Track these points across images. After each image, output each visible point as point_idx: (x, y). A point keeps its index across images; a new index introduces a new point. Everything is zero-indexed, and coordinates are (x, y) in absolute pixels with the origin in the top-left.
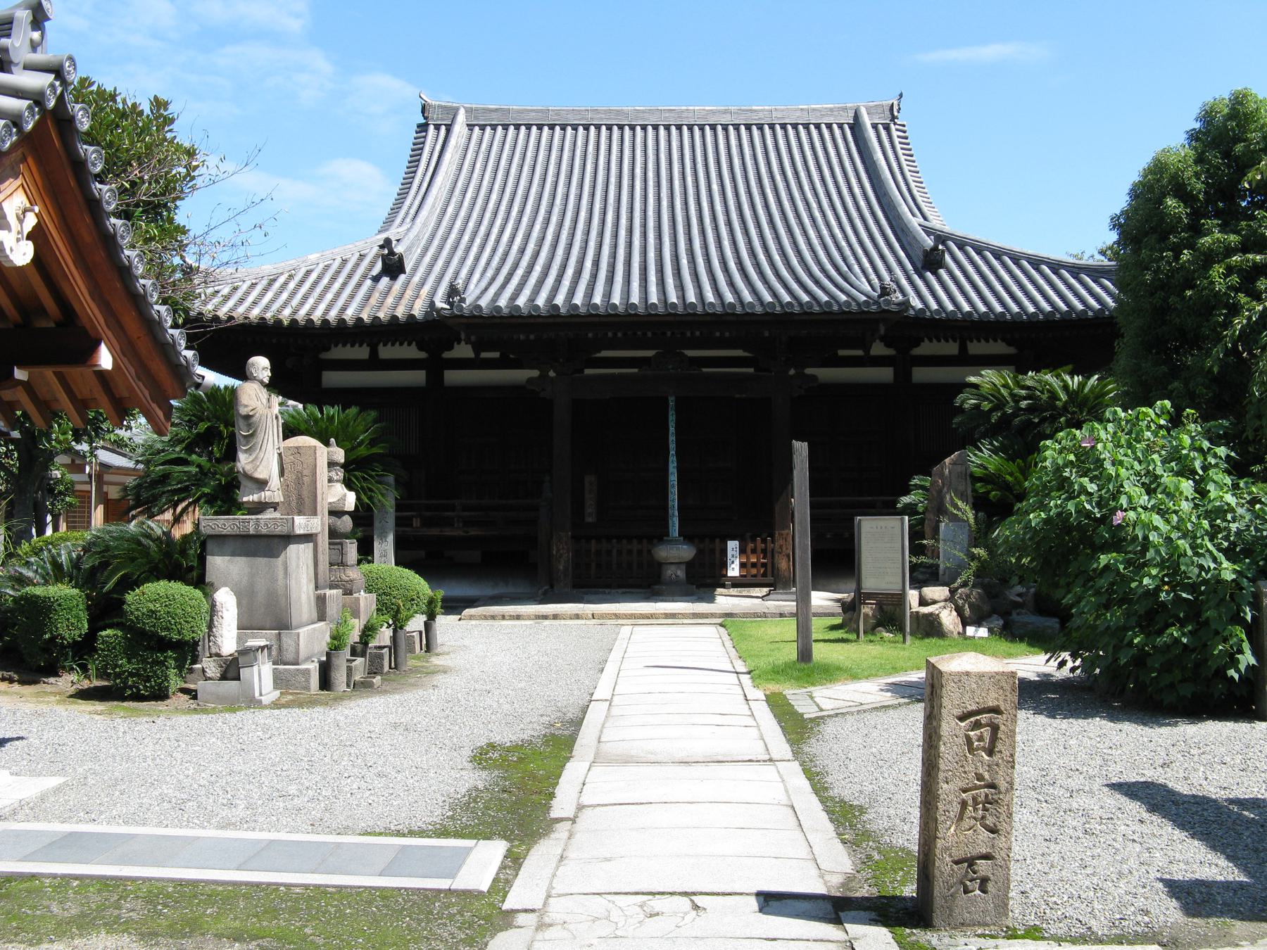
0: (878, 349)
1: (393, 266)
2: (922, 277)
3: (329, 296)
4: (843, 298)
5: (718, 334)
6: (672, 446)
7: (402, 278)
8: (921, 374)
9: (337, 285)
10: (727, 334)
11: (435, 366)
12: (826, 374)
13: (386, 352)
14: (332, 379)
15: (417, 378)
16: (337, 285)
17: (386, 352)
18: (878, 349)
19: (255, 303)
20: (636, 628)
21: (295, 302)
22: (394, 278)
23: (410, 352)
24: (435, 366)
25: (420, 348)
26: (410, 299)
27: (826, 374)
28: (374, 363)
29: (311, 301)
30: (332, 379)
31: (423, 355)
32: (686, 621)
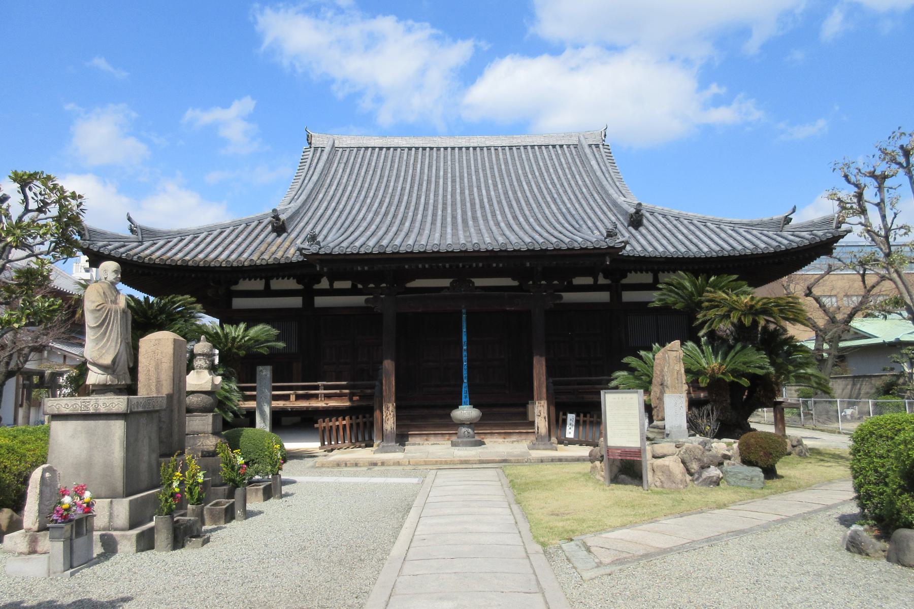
0: (602, 280)
1: (636, 220)
2: (765, 243)
3: (233, 246)
4: (554, 240)
5: (494, 265)
6: (465, 374)
7: (285, 235)
8: (628, 296)
9: (239, 240)
10: (501, 265)
11: (308, 294)
12: (569, 297)
13: (276, 284)
14: (239, 303)
15: (296, 302)
16: (239, 240)
17: (276, 284)
18: (602, 280)
19: (180, 251)
20: (440, 472)
21: (380, 233)
22: (279, 235)
23: (291, 284)
24: (308, 294)
25: (298, 282)
26: (287, 249)
27: (569, 297)
28: (268, 292)
29: (220, 249)
30: (239, 303)
31: (300, 287)
32: (475, 466)
